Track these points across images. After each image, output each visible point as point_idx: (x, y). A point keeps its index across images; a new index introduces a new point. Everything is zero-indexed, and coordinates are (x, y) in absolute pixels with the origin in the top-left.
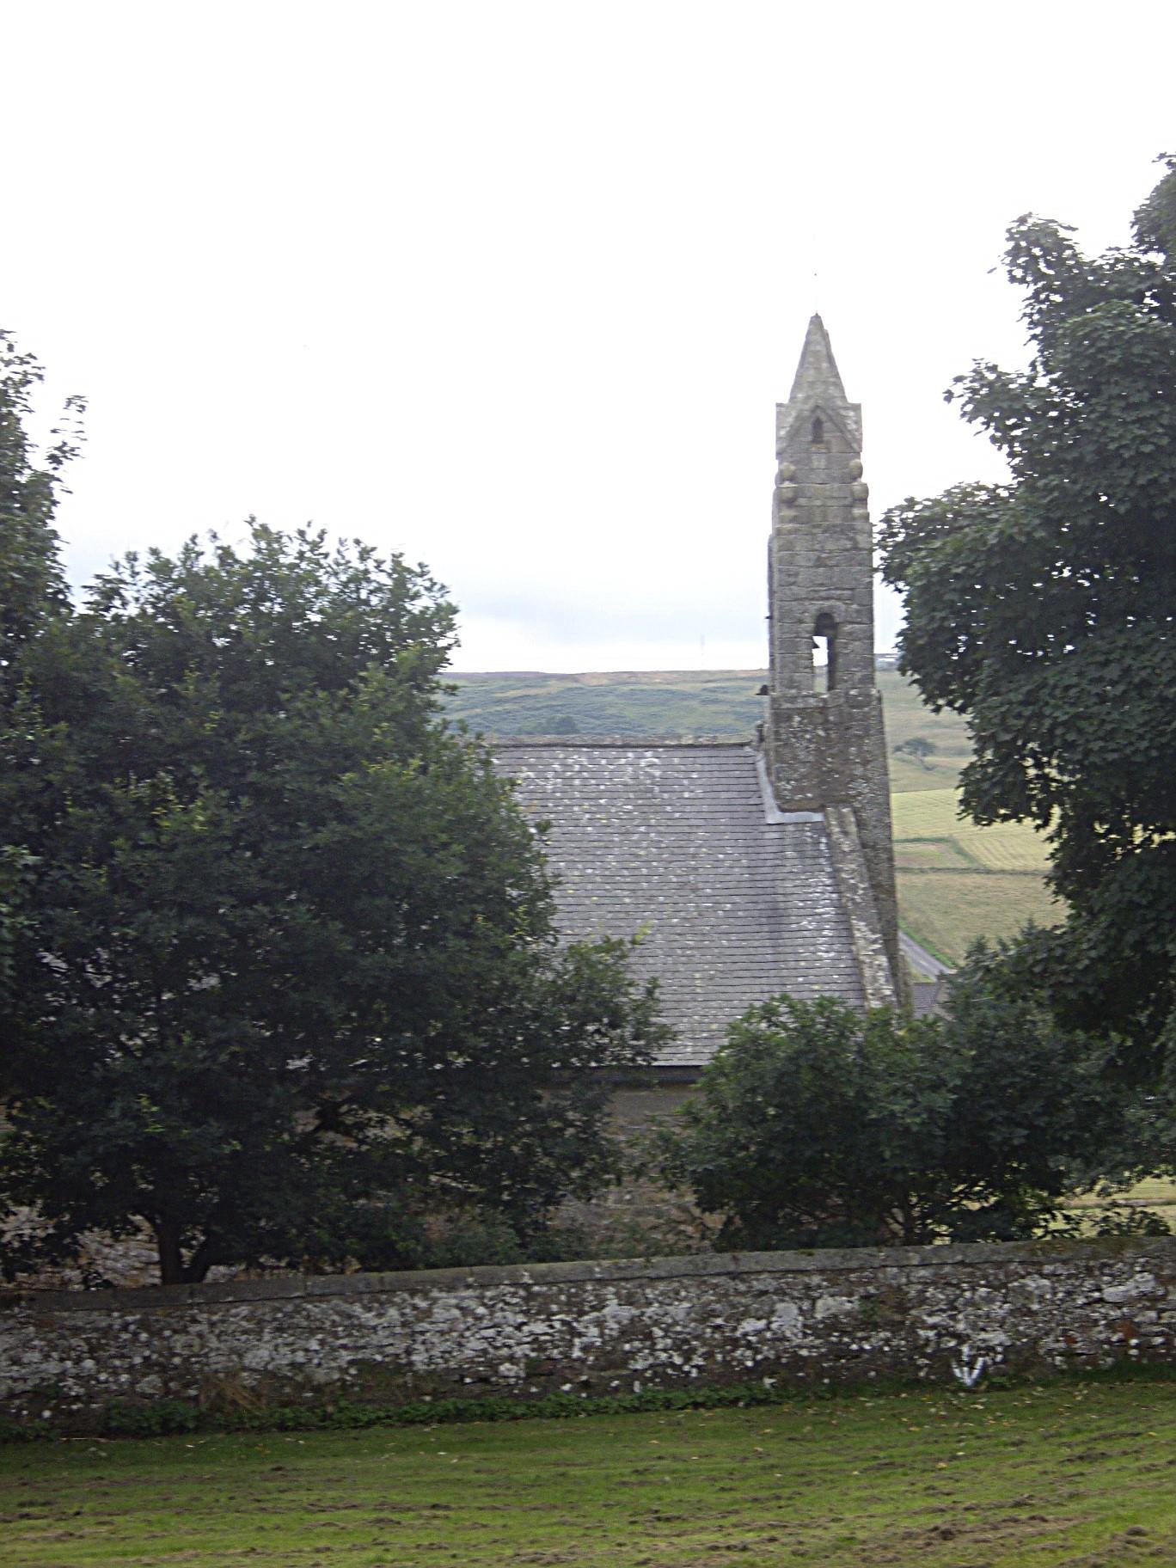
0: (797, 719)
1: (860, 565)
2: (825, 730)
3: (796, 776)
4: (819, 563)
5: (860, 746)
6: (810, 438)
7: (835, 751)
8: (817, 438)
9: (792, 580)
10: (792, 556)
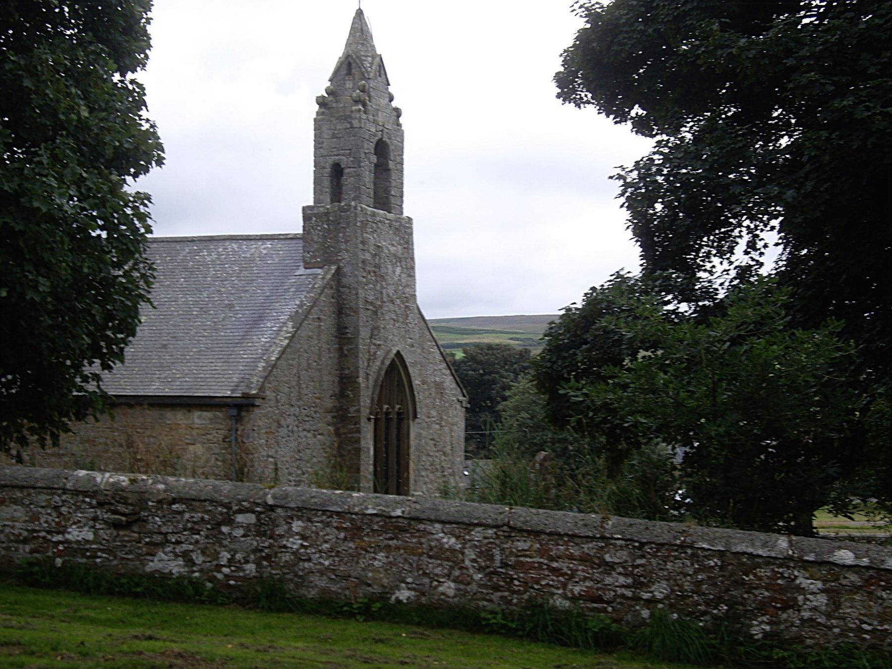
0: (314, 219)
1: (354, 136)
2: (328, 225)
3: (312, 250)
4: (334, 136)
5: (344, 233)
6: (345, 72)
7: (331, 236)
8: (349, 73)
9: (320, 146)
10: (321, 133)
